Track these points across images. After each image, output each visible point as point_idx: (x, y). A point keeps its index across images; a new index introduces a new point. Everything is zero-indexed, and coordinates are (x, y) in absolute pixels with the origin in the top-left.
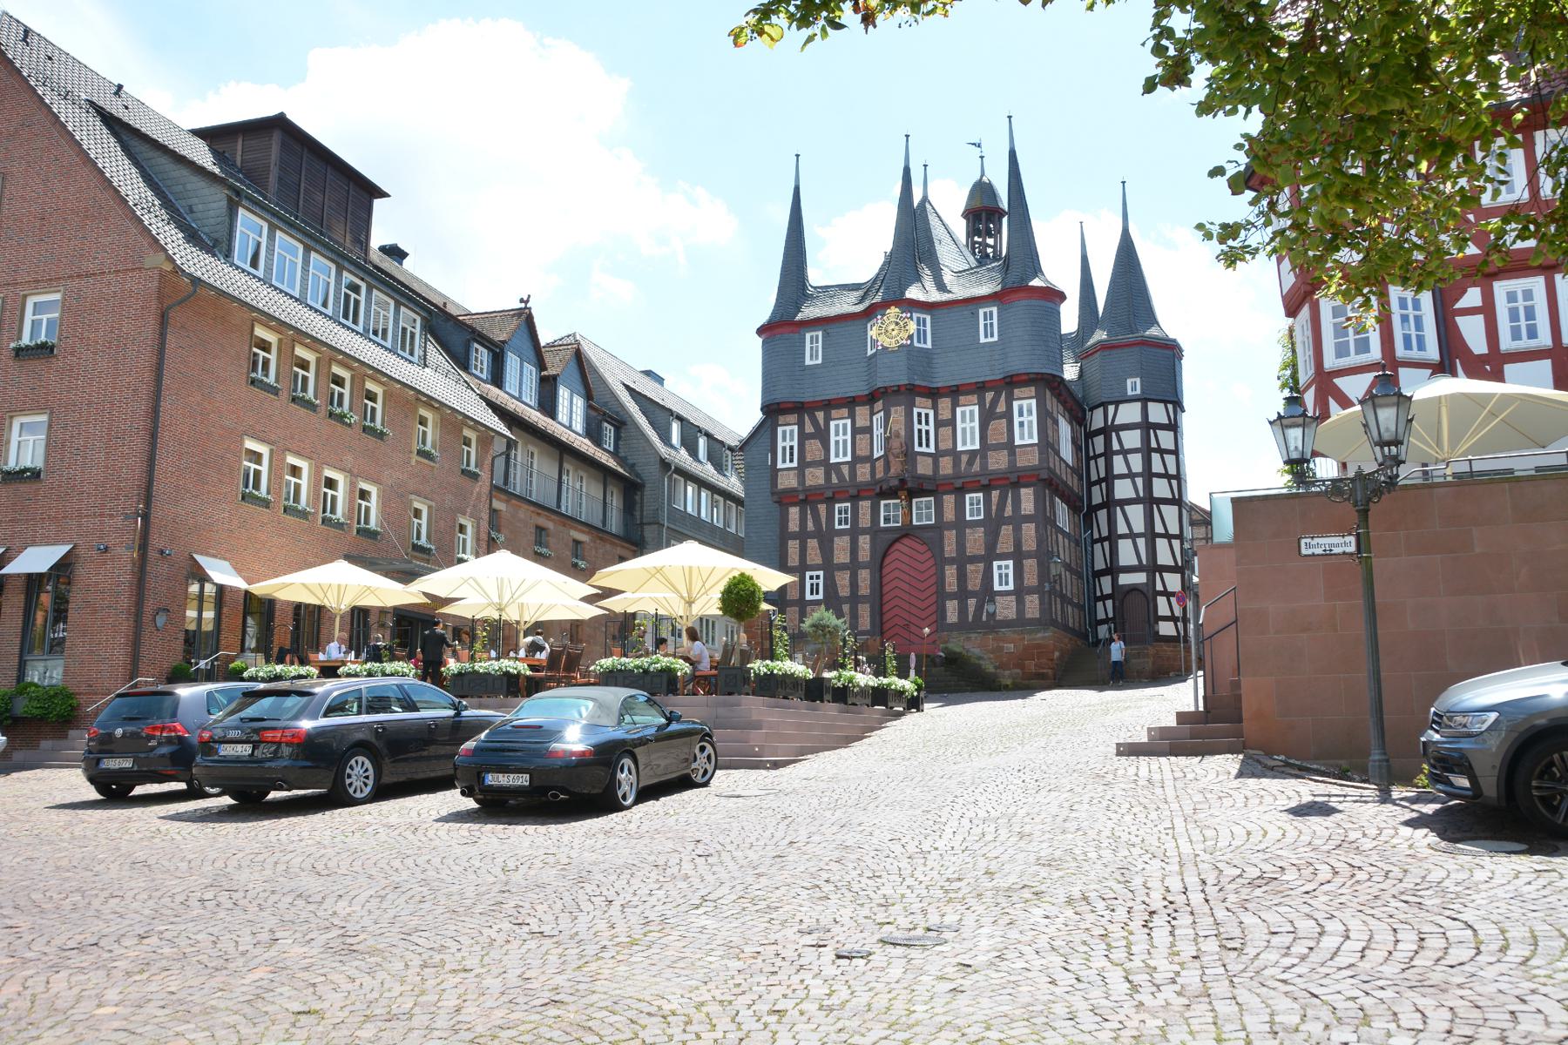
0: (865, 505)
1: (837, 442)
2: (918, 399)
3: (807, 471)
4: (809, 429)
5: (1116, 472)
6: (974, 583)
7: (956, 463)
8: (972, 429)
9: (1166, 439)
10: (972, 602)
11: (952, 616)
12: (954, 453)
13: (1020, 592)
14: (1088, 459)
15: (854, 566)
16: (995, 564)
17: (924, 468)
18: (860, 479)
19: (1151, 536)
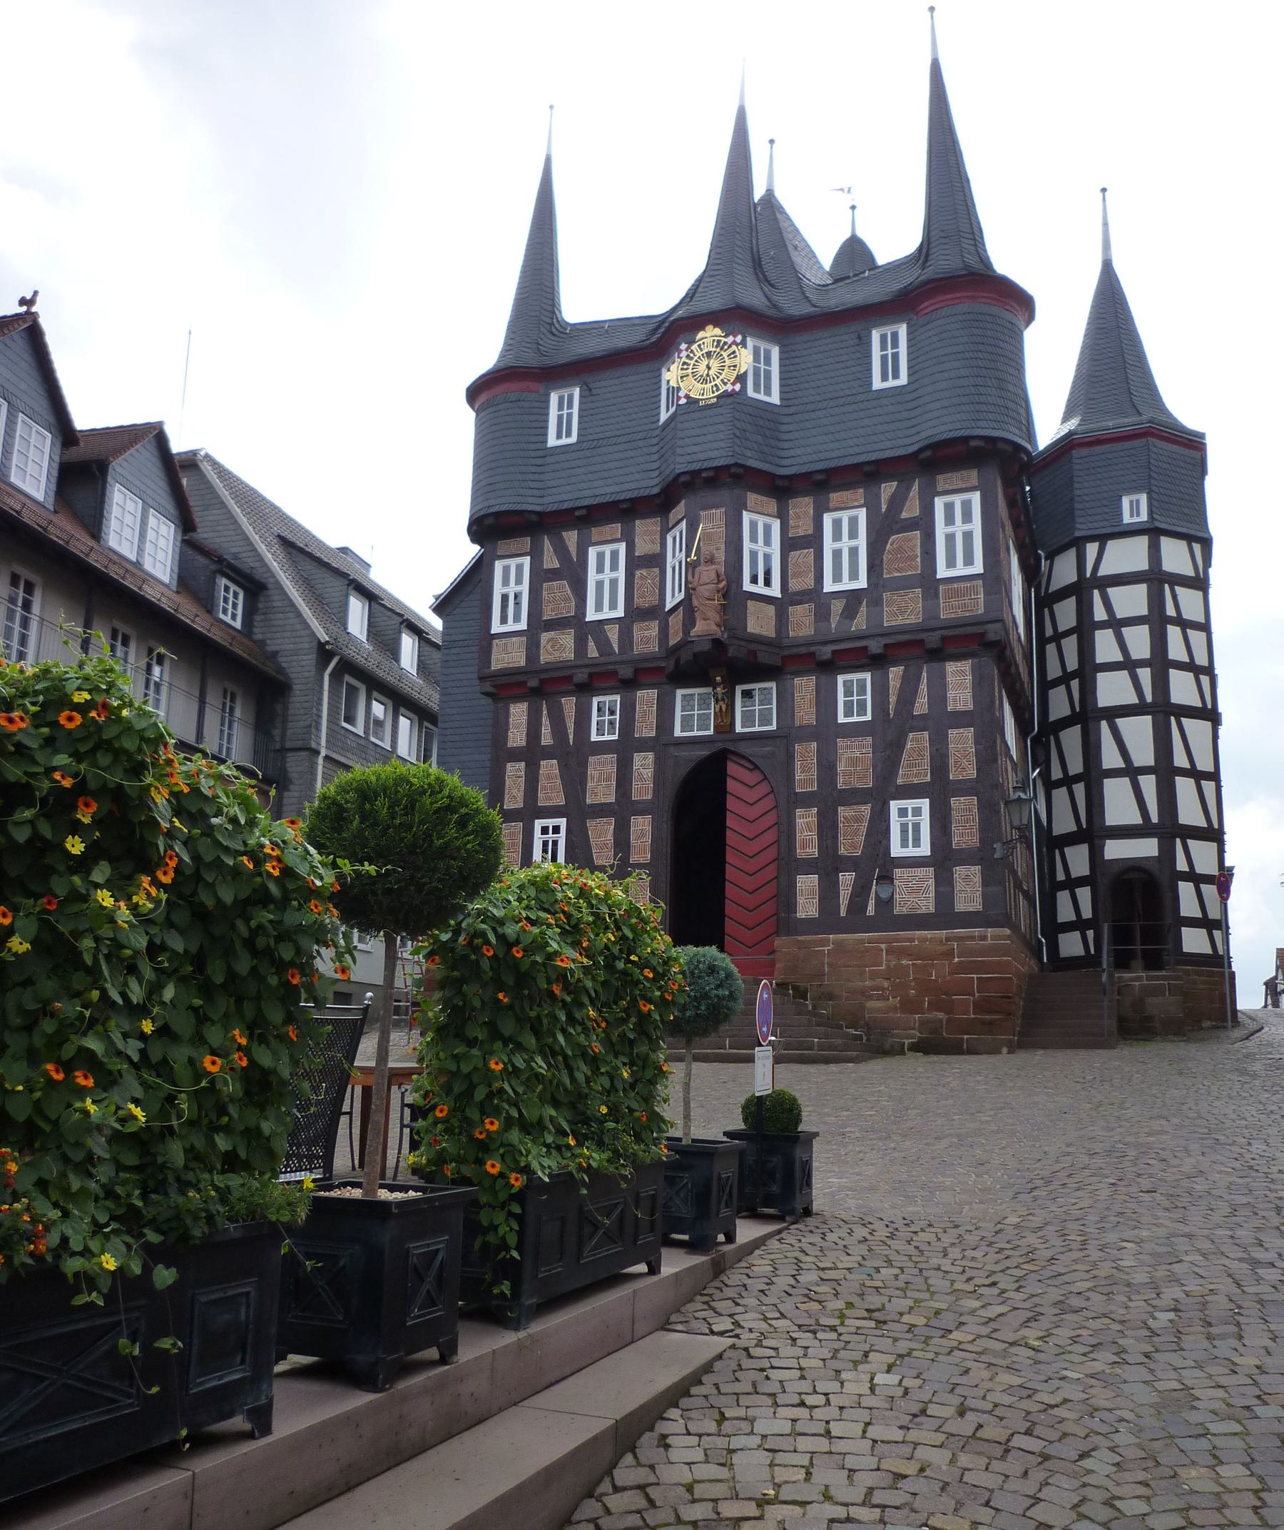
0: (647, 698)
1: (600, 585)
2: (752, 498)
3: (545, 637)
4: (551, 561)
5: (1100, 658)
6: (851, 843)
7: (822, 614)
8: (854, 552)
10: (847, 880)
11: (807, 907)
12: (814, 595)
13: (943, 859)
14: (1043, 642)
15: (622, 810)
16: (894, 805)
17: (759, 623)
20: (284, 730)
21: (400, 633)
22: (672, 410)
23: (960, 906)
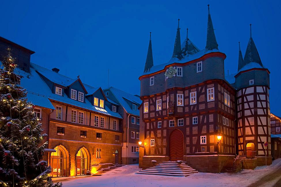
4: (151, 103)
5: (245, 108)
6: (194, 142)
9: (263, 97)
12: (189, 106)
16: (201, 137)
19: (256, 126)
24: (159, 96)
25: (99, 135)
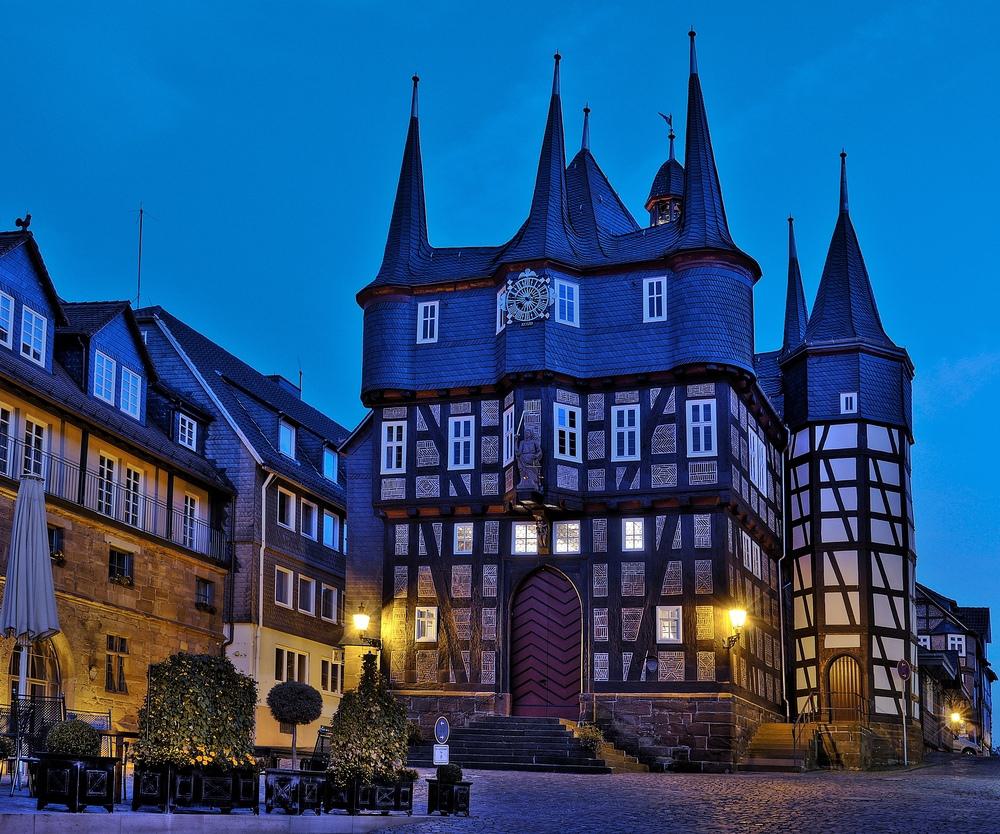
1: (457, 445)
2: (560, 393)
3: (419, 479)
4: (422, 426)
6: (631, 632)
7: (610, 478)
9: (889, 472)
12: (605, 463)
15: (477, 602)
18: (485, 492)
20: (233, 527)
21: (323, 452)
22: (504, 326)
23: (701, 677)
24: (459, 399)
25: (118, 562)
